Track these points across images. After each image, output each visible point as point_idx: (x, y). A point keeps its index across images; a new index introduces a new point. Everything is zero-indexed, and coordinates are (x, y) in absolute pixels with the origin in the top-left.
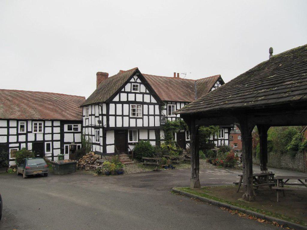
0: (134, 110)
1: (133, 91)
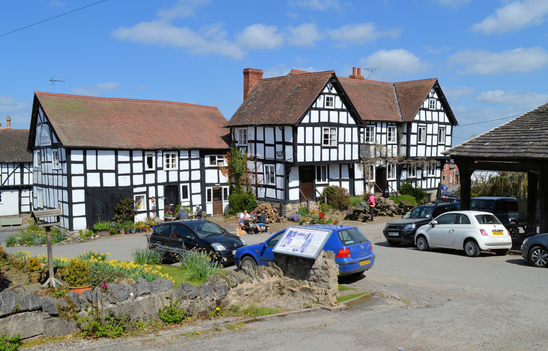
0: (326, 136)
1: (326, 107)
